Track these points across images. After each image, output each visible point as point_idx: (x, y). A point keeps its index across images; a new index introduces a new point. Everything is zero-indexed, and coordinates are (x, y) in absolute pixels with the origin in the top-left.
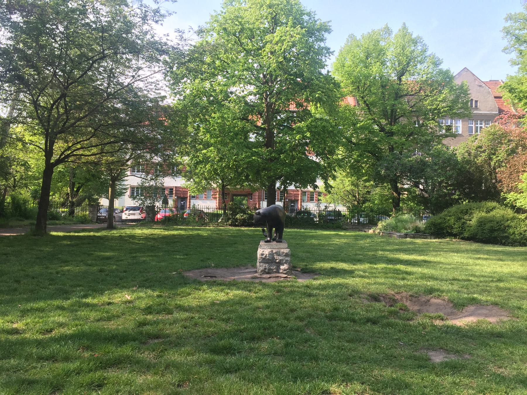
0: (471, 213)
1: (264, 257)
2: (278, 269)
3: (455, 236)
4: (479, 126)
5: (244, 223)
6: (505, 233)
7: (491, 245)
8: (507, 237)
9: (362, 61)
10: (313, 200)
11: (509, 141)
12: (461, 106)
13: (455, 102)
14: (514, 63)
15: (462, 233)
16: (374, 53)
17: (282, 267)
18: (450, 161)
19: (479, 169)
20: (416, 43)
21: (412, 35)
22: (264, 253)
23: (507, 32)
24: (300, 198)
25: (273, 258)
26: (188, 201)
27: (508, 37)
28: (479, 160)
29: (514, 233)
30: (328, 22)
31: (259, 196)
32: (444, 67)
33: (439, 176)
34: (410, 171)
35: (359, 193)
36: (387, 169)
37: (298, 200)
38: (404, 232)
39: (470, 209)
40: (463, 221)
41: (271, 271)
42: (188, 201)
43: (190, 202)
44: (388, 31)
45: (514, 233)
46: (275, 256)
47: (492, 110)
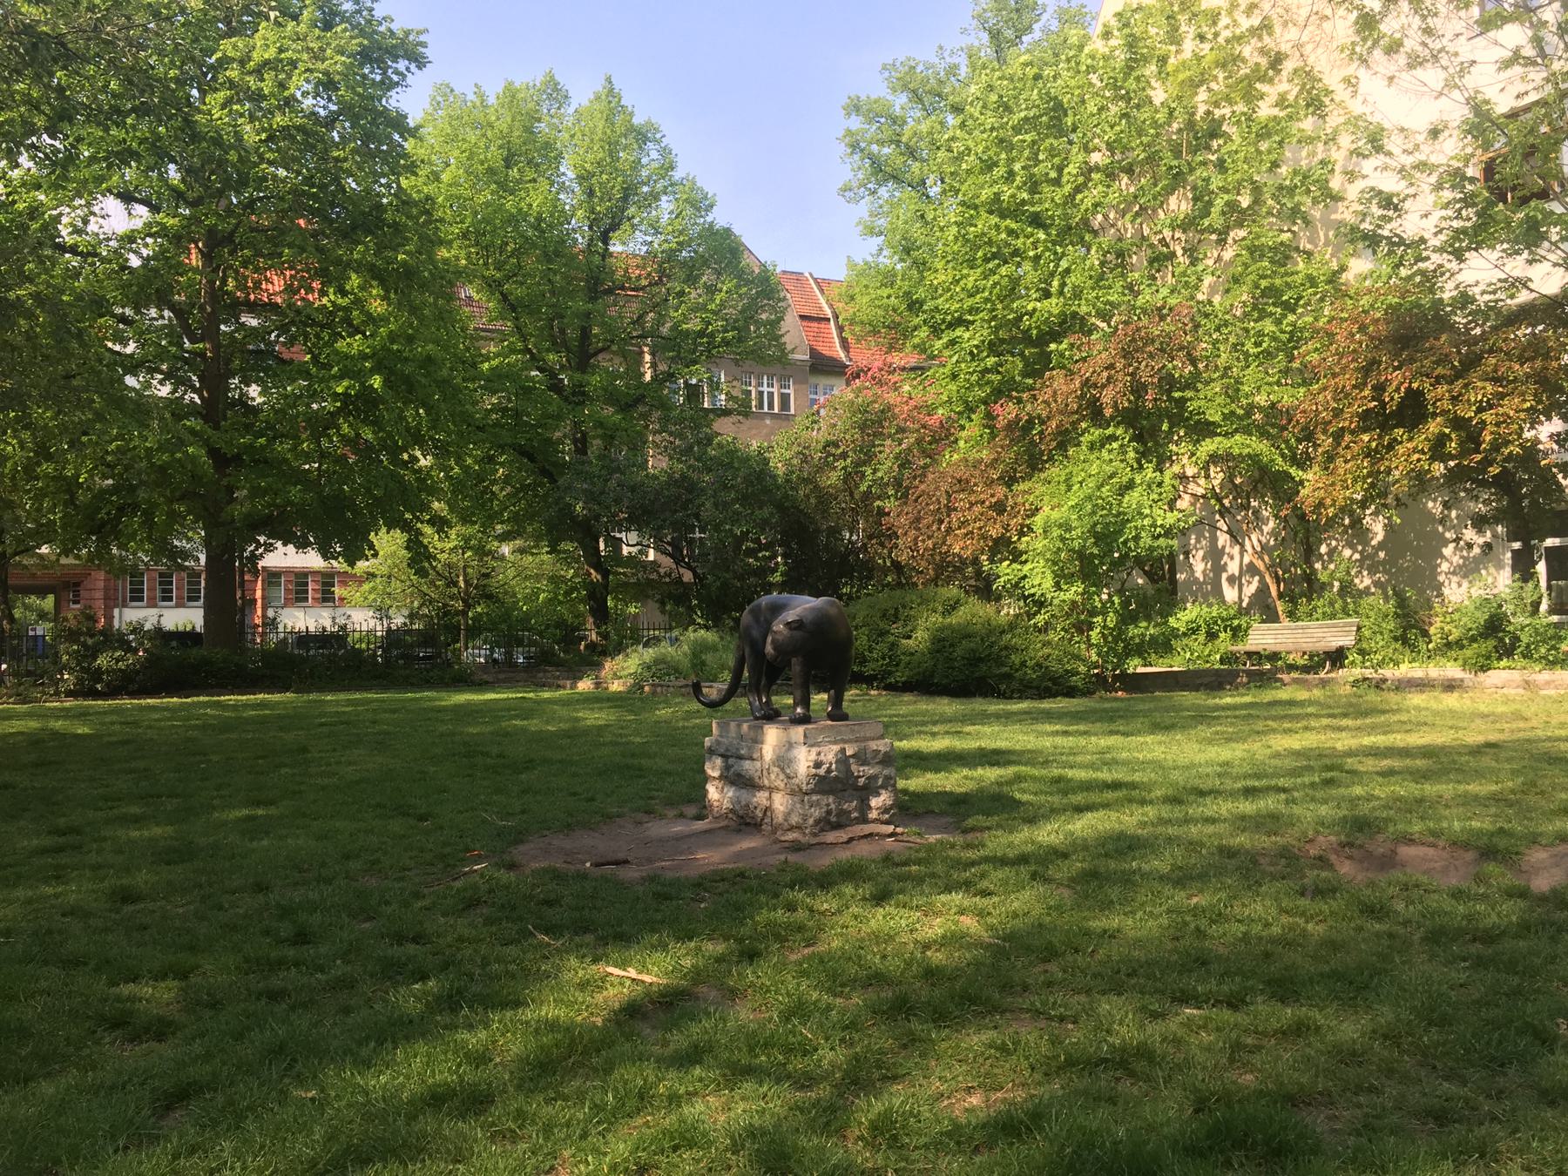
0: (908, 618)
1: (822, 771)
2: (865, 807)
5: (125, 684)
6: (1003, 665)
7: (980, 700)
8: (1008, 676)
9: (491, 171)
10: (141, 599)
11: (901, 430)
13: (749, 314)
14: (872, 231)
15: (890, 673)
16: (522, 152)
17: (875, 802)
18: (754, 481)
19: (824, 498)
20: (645, 139)
21: (631, 114)
22: (822, 757)
24: (259, 594)
25: (849, 772)
27: (857, 157)
29: (1023, 664)
30: (419, 33)
31: (106, 589)
32: (720, 217)
33: (735, 521)
34: (1505, 484)
35: (465, 575)
36: (591, 497)
39: (904, 607)
40: (892, 638)
41: (843, 820)
44: (554, 92)
45: (1023, 664)
46: (854, 767)
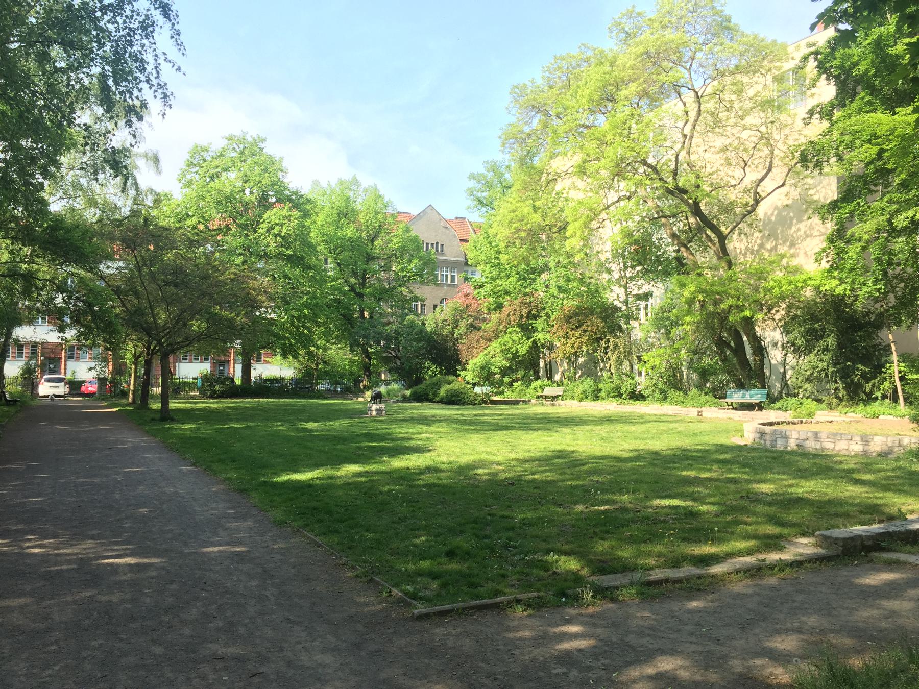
3: (430, 401)
4: (445, 273)
5: (222, 395)
12: (429, 263)
18: (421, 335)
19: (445, 339)
23: (471, 193)
26: (63, 363)
28: (446, 331)
32: (413, 233)
37: (229, 361)
38: (395, 399)
42: (63, 363)
43: (65, 365)
47: (458, 257)
